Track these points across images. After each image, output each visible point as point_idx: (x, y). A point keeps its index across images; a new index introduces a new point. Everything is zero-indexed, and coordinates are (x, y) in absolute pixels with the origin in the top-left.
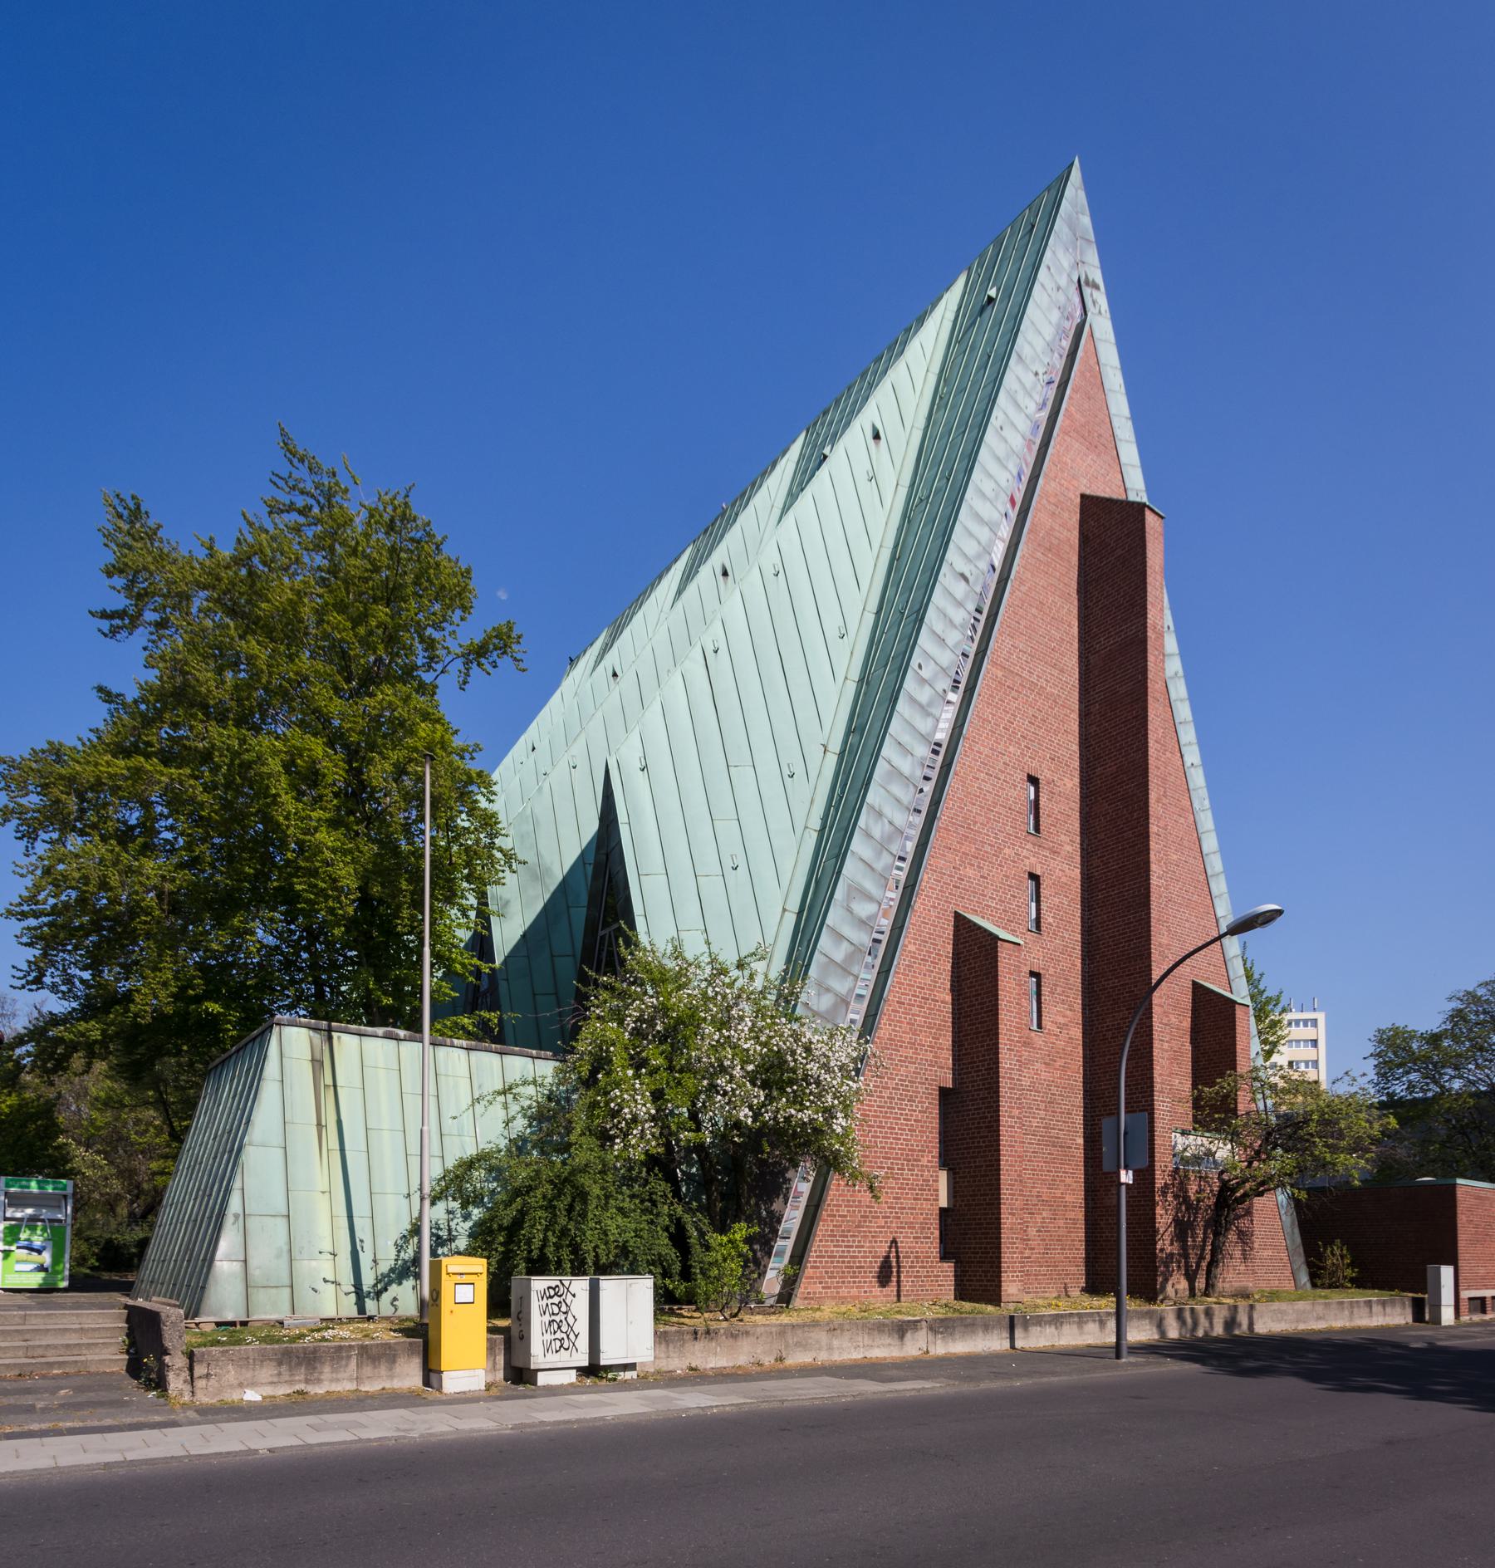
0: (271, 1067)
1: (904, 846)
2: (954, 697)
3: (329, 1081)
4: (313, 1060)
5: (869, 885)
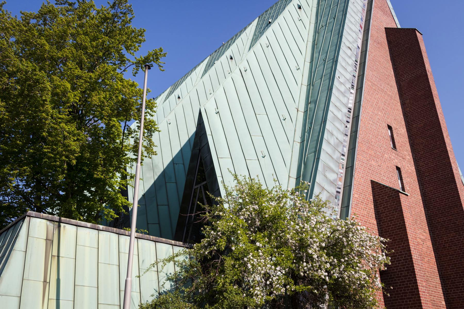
0: (20, 243)
1: (343, 150)
2: (354, 91)
3: (55, 253)
4: (47, 239)
5: (332, 165)
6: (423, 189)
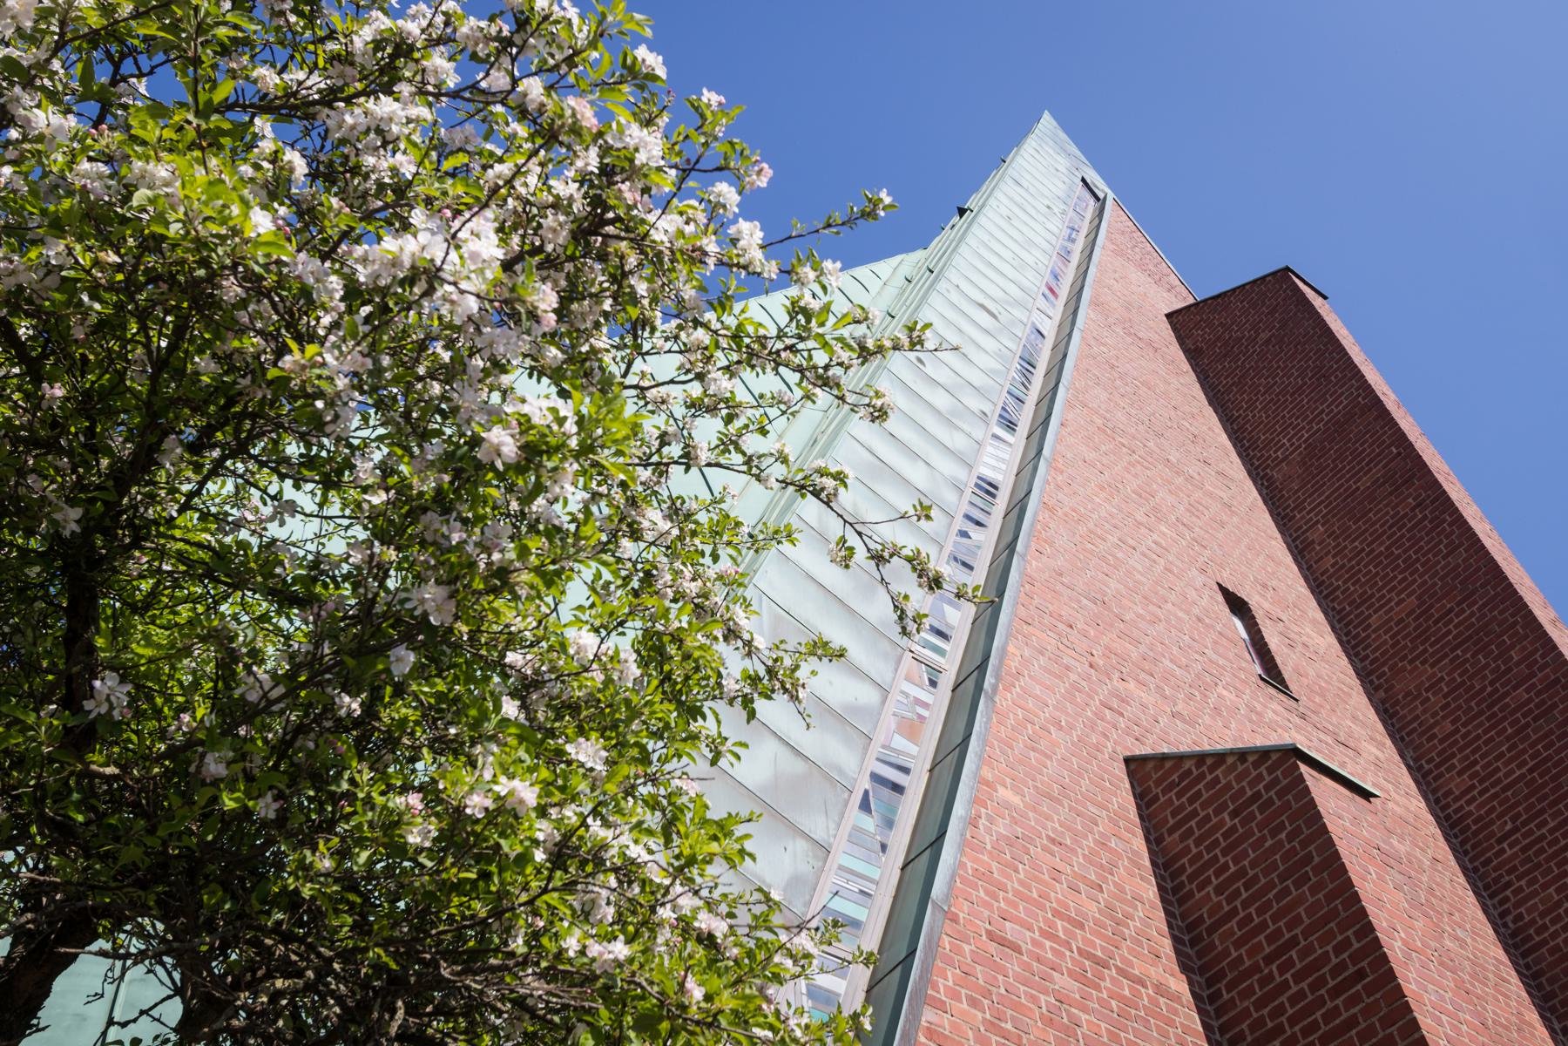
6: (1502, 915)
